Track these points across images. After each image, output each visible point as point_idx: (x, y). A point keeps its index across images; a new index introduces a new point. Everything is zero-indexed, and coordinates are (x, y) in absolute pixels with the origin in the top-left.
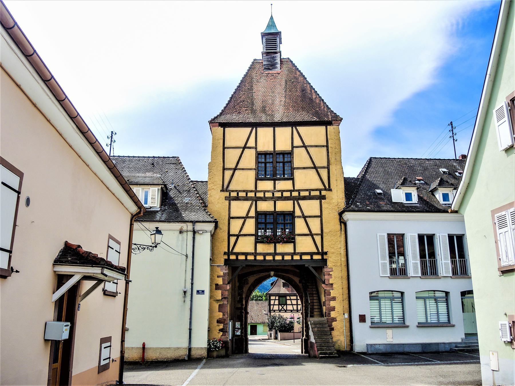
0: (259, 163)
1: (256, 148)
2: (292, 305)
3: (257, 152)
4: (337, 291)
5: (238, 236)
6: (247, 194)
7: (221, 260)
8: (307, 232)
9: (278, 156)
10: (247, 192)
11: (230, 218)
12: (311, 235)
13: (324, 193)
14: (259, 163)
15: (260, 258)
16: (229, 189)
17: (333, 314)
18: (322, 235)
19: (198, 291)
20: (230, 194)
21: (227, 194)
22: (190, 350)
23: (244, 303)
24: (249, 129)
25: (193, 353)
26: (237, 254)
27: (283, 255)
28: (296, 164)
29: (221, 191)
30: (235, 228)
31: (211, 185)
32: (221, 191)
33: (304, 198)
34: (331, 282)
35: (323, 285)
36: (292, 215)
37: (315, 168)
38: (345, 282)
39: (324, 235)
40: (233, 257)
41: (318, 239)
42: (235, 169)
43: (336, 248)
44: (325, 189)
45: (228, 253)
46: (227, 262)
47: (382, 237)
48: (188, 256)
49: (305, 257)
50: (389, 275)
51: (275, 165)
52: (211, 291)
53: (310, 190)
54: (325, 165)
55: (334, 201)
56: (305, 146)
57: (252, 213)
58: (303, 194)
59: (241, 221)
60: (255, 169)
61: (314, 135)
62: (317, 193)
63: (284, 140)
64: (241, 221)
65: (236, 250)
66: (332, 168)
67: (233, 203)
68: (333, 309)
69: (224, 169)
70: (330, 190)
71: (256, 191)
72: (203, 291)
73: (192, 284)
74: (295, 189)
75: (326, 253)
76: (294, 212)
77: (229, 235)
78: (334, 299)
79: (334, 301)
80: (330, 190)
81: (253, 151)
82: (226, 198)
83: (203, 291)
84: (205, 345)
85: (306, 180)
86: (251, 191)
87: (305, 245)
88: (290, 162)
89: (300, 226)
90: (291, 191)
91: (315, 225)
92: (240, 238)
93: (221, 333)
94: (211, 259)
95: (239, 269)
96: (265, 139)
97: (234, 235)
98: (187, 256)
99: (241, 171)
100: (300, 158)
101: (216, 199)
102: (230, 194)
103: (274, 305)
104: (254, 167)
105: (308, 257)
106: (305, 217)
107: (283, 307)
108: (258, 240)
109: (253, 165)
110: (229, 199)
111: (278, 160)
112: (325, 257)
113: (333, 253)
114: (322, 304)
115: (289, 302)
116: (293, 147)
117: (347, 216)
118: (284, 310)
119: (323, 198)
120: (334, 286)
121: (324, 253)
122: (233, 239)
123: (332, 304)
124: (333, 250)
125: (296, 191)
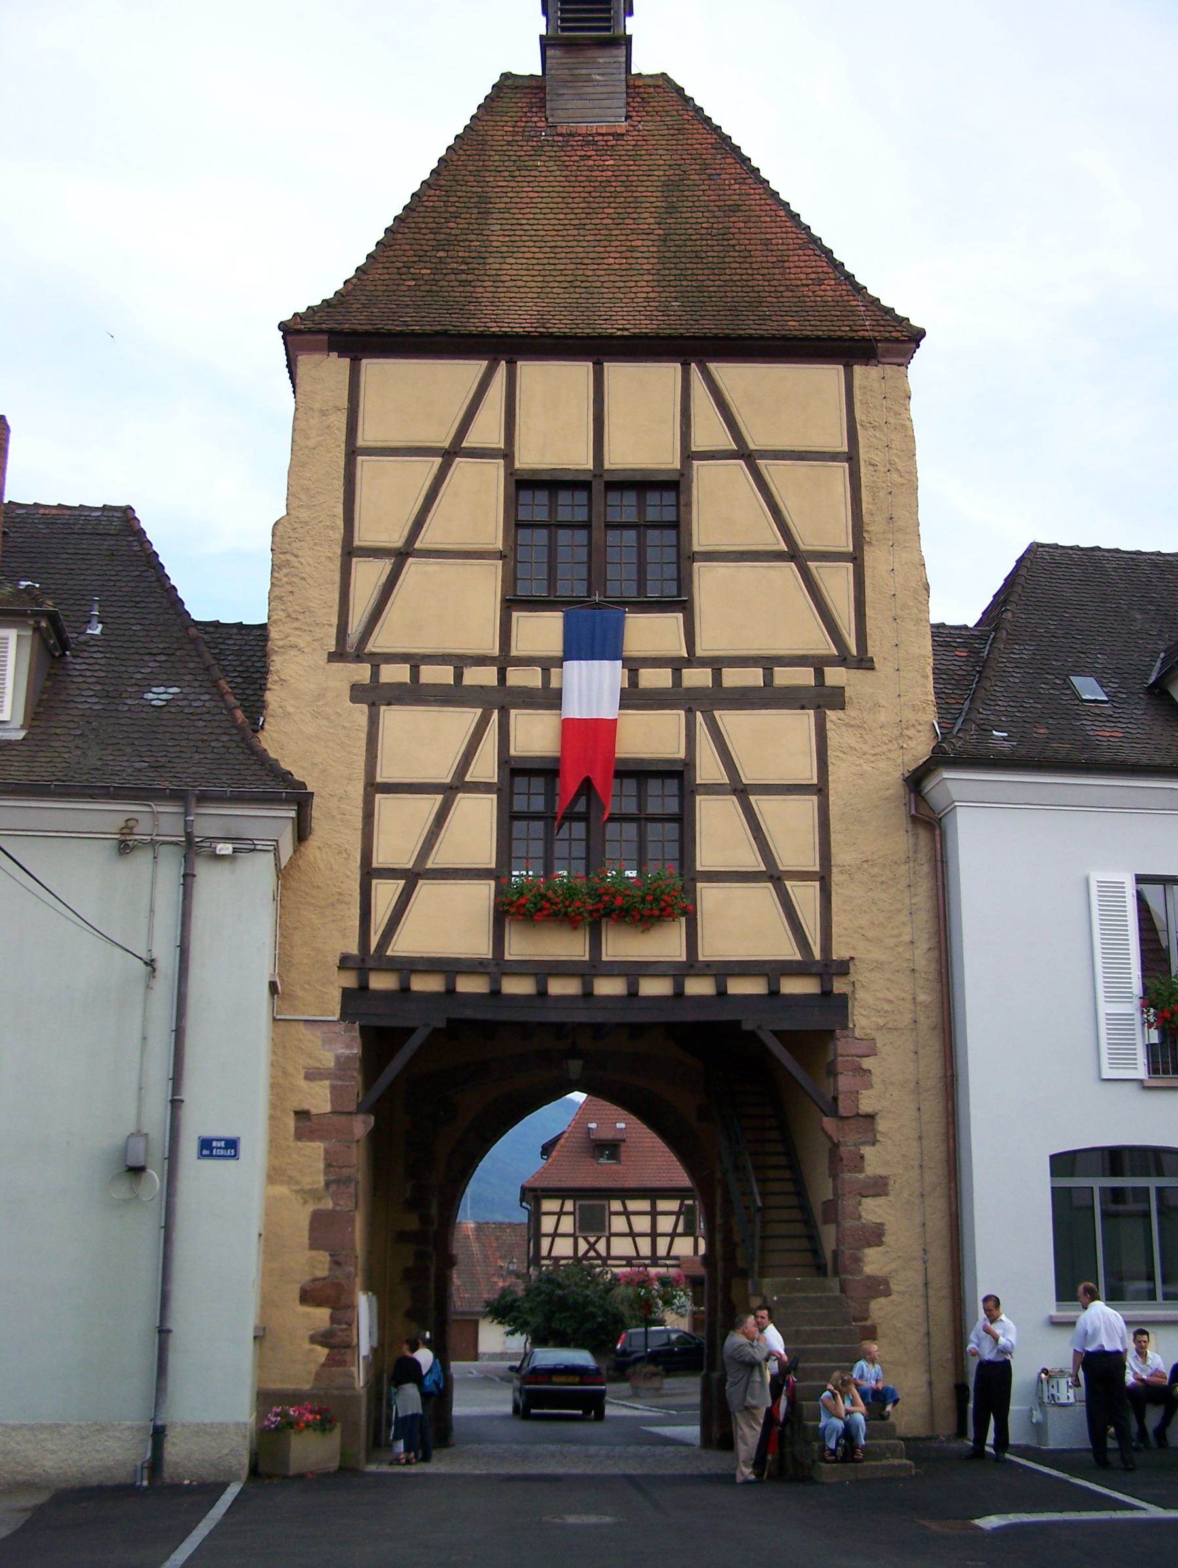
0: (519, 525)
1: (507, 454)
2: (632, 1234)
3: (510, 471)
4: (893, 1151)
5: (412, 877)
6: (459, 676)
7: (326, 994)
8: (752, 861)
9: (614, 498)
10: (460, 662)
11: (374, 788)
12: (774, 877)
13: (835, 676)
14: (519, 525)
15: (516, 986)
16: (371, 647)
17: (874, 1261)
18: (824, 878)
19: (206, 1146)
20: (375, 673)
21: (363, 673)
22: (159, 1434)
23: (434, 1211)
24: (475, 368)
25: (174, 1450)
26: (408, 967)
27: (634, 971)
28: (703, 537)
29: (333, 657)
30: (400, 831)
31: (287, 629)
32: (333, 657)
33: (744, 699)
34: (866, 1106)
35: (828, 1123)
36: (678, 775)
37: (794, 554)
38: (933, 1107)
39: (836, 877)
40: (381, 982)
41: (805, 896)
42: (402, 555)
43: (891, 942)
44: (843, 660)
45: (361, 963)
46: (355, 1001)
47: (1111, 889)
48: (159, 965)
49: (738, 987)
50: (1141, 1072)
51: (598, 544)
52: (275, 1146)
53: (768, 663)
54: (846, 544)
55: (882, 717)
56: (745, 454)
57: (486, 767)
58: (733, 678)
59: (430, 804)
60: (502, 556)
61: (788, 401)
62: (804, 677)
63: (643, 416)
64: (430, 804)
65: (401, 947)
66: (876, 559)
67: (394, 718)
68: (876, 1235)
69: (350, 551)
70: (864, 663)
71: (504, 661)
72: (232, 1144)
73: (176, 1104)
74: (699, 652)
75: (843, 968)
76: (689, 764)
77: (369, 873)
78: (879, 1187)
79: (881, 1201)
80: (864, 663)
81: (495, 471)
82: (358, 693)
83: (232, 1144)
84: (239, 1410)
85: (745, 611)
86: (481, 661)
87: (739, 926)
88: (675, 525)
89: (719, 834)
90: (677, 665)
91: (791, 827)
92: (424, 889)
93: (322, 1352)
94: (273, 987)
95: (416, 1041)
96: (555, 416)
97: (390, 873)
98: (150, 963)
99: (431, 567)
100: (722, 508)
101: (307, 715)
102: (375, 673)
103: (555, 1235)
104: (499, 545)
105: (753, 987)
106: (741, 791)
107: (592, 1246)
108: (510, 910)
109: (493, 535)
110: (373, 696)
111: (614, 516)
112: (839, 986)
113: (879, 966)
114: (818, 1212)
115: (618, 1224)
116: (688, 456)
117: (953, 783)
118: (599, 1256)
119: (834, 699)
120: (882, 1125)
121: (830, 969)
122: (385, 893)
123: (872, 1210)
124: (877, 954)
125: (704, 662)
